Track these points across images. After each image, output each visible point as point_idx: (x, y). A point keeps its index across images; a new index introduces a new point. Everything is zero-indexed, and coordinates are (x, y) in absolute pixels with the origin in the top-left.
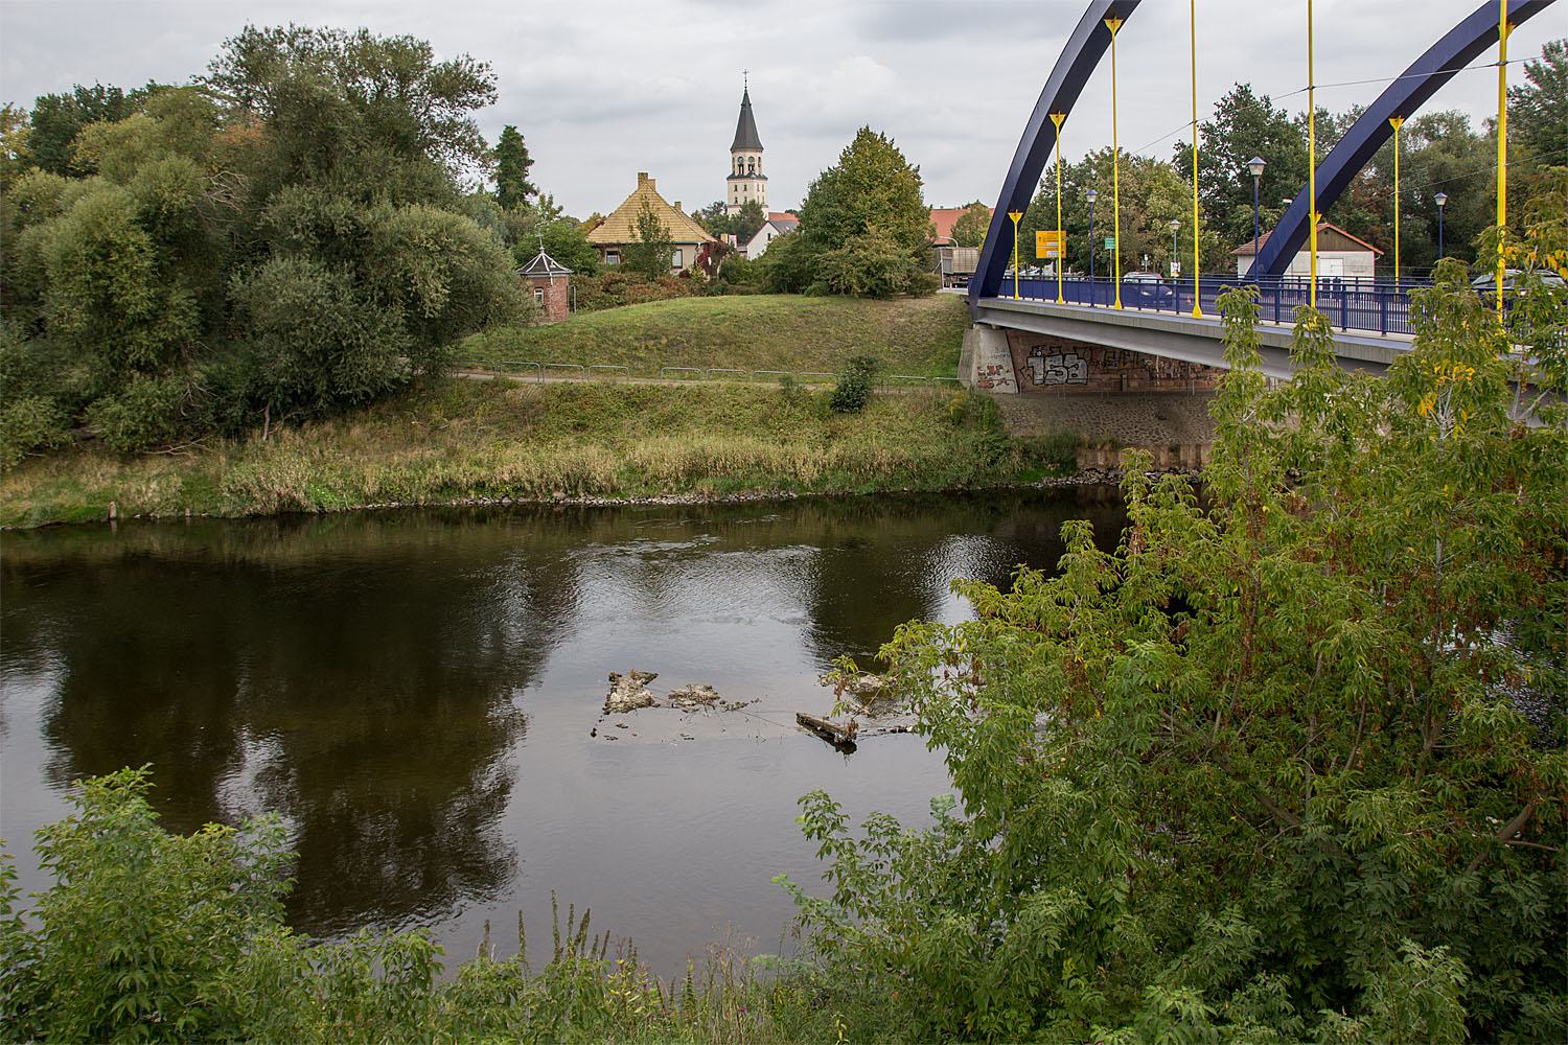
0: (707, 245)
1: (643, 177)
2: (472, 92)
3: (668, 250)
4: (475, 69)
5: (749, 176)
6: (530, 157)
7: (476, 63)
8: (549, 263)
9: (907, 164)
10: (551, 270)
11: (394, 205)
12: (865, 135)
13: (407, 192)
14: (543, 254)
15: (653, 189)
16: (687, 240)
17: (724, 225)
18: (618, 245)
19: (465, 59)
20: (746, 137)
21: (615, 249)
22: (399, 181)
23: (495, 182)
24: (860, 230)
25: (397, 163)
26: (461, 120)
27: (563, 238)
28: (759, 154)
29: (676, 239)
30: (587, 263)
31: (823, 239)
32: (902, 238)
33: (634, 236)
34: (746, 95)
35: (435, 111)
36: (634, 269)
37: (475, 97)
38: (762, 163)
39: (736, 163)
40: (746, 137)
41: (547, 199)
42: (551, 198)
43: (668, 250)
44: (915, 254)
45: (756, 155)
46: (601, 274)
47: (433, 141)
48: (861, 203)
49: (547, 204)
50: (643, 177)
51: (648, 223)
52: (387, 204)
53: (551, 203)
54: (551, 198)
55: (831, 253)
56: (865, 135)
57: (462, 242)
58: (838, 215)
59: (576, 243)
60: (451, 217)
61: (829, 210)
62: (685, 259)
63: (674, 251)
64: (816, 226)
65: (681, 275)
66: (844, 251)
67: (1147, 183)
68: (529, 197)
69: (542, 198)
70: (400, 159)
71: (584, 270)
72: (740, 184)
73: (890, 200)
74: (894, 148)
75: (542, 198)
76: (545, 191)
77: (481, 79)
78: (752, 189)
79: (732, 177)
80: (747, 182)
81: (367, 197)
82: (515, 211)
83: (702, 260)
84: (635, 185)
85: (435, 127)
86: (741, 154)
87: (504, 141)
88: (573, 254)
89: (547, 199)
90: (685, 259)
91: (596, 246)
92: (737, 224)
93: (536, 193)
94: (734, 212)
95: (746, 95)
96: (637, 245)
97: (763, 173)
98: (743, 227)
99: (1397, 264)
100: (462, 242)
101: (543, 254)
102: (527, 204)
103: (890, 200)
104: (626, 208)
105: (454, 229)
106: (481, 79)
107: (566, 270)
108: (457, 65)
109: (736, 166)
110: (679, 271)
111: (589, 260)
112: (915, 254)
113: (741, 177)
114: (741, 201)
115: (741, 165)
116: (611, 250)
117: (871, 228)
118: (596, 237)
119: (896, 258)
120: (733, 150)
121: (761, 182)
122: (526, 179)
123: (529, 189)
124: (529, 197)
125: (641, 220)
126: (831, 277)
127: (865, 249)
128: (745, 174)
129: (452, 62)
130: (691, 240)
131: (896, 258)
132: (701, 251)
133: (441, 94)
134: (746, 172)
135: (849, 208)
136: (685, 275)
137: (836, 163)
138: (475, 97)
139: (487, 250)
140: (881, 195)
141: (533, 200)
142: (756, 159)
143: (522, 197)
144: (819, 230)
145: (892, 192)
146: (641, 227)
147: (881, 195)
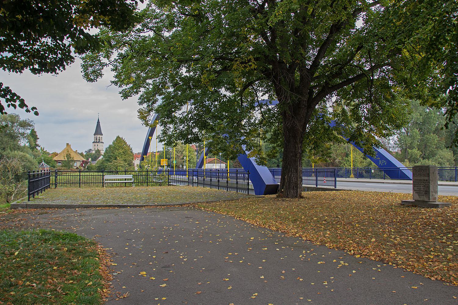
0: (83, 161)
1: (68, 144)
2: (29, 126)
3: (73, 162)
4: (30, 122)
5: (99, 142)
6: (38, 137)
7: (30, 120)
8: (45, 164)
9: (127, 144)
10: (45, 166)
11: (11, 151)
12: (118, 137)
13: (14, 148)
14: (43, 162)
15: (70, 147)
16: (78, 160)
17: (90, 156)
18: (61, 161)
19: (28, 119)
20: (98, 131)
21: (60, 162)
22: (12, 146)
23: (28, 143)
24: (116, 159)
25: (11, 142)
26: (26, 132)
27: (47, 159)
28: (101, 136)
29: (75, 160)
30: (53, 165)
31: (108, 160)
32: (125, 161)
33: (65, 159)
34: (98, 119)
35: (20, 130)
36: (65, 166)
37: (29, 128)
38: (102, 139)
39: (95, 139)
40: (98, 131)
41: (42, 148)
42: (44, 148)
43: (73, 162)
44: (128, 164)
45: (101, 136)
46: (57, 168)
47: (19, 137)
48: (116, 152)
49: (42, 149)
50: (68, 144)
51: (68, 156)
52: (9, 151)
53: (44, 149)
54: (44, 148)
55: (109, 164)
56: (118, 137)
57: (27, 159)
58: (111, 155)
59: (51, 160)
60: (25, 154)
61: (109, 154)
62: (78, 164)
63: (75, 162)
64: (106, 157)
65: (76, 168)
66: (112, 163)
67: (183, 148)
68: (37, 148)
69: (41, 148)
70: (12, 141)
71: (53, 166)
72: (96, 144)
73: (123, 152)
74: (125, 140)
75: (41, 148)
76: (42, 146)
77: (31, 124)
78: (99, 145)
79: (94, 142)
80: (98, 144)
81: (4, 149)
82: (34, 151)
83: (82, 165)
84: (66, 146)
85: (20, 133)
86: (96, 136)
87: (31, 133)
88: (50, 162)
89: (42, 148)
90: (78, 164)
91: (55, 161)
92: (94, 155)
93: (39, 147)
94: (94, 152)
95: (98, 119)
96: (66, 161)
97: (103, 141)
98: (95, 156)
99: (313, 166)
100: (27, 159)
101: (43, 162)
102: (37, 149)
103: (123, 152)
104: (63, 152)
105: (25, 157)
106: (31, 124)
107: (49, 166)
108: (26, 120)
109: (95, 139)
110: (76, 167)
111: (54, 164)
112: (128, 164)
113: (97, 142)
114: (96, 149)
115: (97, 139)
116: (59, 162)
117: (118, 158)
118: (56, 158)
119: (123, 165)
120: (94, 135)
121: (102, 144)
122: (37, 143)
123: (37, 145)
124: (37, 148)
125: (67, 155)
126: (109, 169)
127: (117, 163)
128: (95, 142)
129: (25, 120)
130: (79, 160)
131: (123, 165)
132: (81, 163)
133: (21, 127)
134: (98, 141)
135: (114, 154)
136: (77, 168)
137: (111, 144)
138: (29, 128)
139: (32, 161)
140: (121, 151)
141: (39, 148)
142: (101, 137)
143: (36, 147)
144: (107, 159)
145: (123, 151)
146: (67, 157)
147: (121, 151)
